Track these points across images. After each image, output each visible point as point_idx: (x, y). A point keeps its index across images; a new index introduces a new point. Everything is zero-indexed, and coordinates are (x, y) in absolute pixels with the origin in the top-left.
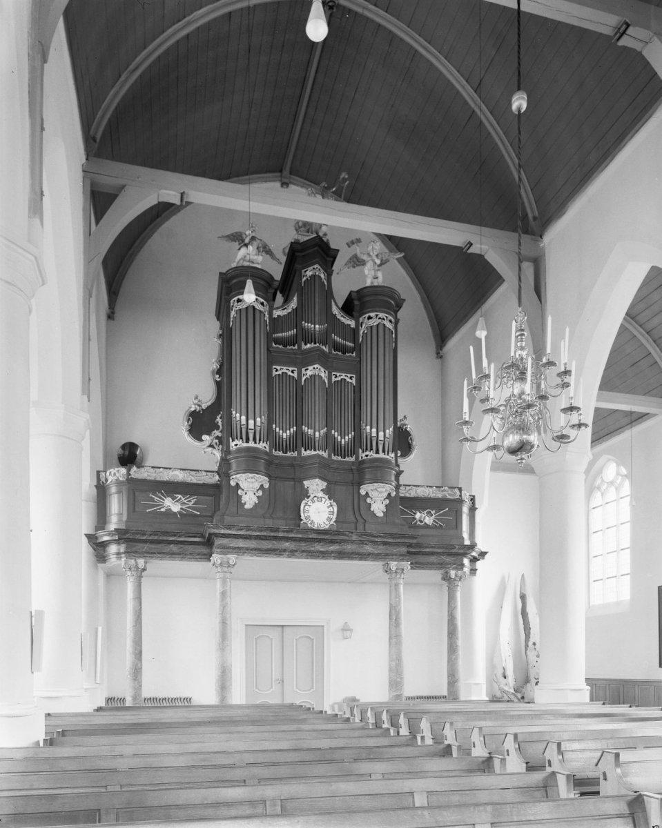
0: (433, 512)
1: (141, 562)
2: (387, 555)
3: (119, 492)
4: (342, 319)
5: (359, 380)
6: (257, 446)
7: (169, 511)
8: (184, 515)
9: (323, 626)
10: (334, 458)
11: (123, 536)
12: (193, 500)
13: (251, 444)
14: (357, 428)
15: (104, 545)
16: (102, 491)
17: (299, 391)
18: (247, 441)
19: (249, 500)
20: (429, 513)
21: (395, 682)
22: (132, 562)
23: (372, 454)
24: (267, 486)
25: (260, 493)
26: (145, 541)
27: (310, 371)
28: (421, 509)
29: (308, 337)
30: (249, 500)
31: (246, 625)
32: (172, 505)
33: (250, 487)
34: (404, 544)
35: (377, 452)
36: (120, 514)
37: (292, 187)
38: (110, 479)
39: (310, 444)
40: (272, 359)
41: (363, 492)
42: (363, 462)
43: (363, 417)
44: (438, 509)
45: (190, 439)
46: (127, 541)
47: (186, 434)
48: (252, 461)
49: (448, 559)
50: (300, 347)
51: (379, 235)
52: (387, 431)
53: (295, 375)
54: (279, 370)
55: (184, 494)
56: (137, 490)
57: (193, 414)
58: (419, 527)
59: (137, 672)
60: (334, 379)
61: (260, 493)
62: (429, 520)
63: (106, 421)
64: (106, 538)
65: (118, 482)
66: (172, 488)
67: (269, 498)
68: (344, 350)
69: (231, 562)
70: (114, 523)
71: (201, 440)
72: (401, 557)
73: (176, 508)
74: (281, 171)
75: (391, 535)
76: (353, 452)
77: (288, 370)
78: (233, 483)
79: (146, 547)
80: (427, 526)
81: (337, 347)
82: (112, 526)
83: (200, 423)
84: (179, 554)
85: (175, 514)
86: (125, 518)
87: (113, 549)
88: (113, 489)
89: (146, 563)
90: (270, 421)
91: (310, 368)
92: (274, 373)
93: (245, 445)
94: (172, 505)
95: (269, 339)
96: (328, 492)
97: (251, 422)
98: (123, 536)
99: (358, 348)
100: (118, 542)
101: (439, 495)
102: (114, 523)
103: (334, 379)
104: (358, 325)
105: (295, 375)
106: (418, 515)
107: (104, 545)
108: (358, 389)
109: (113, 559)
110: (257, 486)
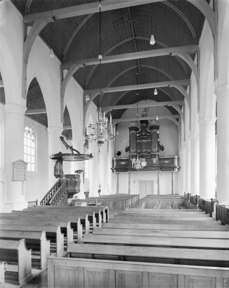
1: (118, 172)
5: (151, 141)
7: (122, 164)
8: (125, 164)
10: (147, 154)
11: (115, 168)
12: (126, 162)
13: (133, 154)
16: (113, 161)
17: (141, 144)
20: (168, 161)
21: (129, 191)
22: (117, 172)
23: (153, 153)
26: (119, 169)
27: (142, 141)
28: (165, 160)
29: (142, 135)
31: (139, 181)
37: (147, 100)
38: (114, 159)
39: (143, 153)
40: (137, 139)
41: (152, 160)
42: (152, 155)
43: (152, 147)
47: (125, 151)
49: (171, 169)
51: (164, 106)
53: (141, 141)
55: (125, 161)
56: (118, 161)
59: (118, 190)
60: (147, 141)
62: (167, 162)
64: (114, 169)
65: (115, 160)
68: (149, 136)
69: (130, 172)
70: (115, 167)
72: (159, 170)
73: (123, 164)
74: (144, 98)
77: (140, 141)
78: (131, 160)
79: (119, 170)
80: (167, 163)
81: (147, 136)
82: (115, 167)
85: (123, 165)
87: (115, 170)
88: (115, 161)
90: (137, 149)
92: (137, 142)
93: (132, 154)
96: (146, 161)
97: (133, 151)
98: (115, 168)
99: (151, 135)
100: (115, 169)
101: (170, 157)
103: (147, 141)
104: (151, 131)
105: (141, 141)
106: (165, 161)
108: (151, 142)
109: (115, 172)
110: (156, 160)
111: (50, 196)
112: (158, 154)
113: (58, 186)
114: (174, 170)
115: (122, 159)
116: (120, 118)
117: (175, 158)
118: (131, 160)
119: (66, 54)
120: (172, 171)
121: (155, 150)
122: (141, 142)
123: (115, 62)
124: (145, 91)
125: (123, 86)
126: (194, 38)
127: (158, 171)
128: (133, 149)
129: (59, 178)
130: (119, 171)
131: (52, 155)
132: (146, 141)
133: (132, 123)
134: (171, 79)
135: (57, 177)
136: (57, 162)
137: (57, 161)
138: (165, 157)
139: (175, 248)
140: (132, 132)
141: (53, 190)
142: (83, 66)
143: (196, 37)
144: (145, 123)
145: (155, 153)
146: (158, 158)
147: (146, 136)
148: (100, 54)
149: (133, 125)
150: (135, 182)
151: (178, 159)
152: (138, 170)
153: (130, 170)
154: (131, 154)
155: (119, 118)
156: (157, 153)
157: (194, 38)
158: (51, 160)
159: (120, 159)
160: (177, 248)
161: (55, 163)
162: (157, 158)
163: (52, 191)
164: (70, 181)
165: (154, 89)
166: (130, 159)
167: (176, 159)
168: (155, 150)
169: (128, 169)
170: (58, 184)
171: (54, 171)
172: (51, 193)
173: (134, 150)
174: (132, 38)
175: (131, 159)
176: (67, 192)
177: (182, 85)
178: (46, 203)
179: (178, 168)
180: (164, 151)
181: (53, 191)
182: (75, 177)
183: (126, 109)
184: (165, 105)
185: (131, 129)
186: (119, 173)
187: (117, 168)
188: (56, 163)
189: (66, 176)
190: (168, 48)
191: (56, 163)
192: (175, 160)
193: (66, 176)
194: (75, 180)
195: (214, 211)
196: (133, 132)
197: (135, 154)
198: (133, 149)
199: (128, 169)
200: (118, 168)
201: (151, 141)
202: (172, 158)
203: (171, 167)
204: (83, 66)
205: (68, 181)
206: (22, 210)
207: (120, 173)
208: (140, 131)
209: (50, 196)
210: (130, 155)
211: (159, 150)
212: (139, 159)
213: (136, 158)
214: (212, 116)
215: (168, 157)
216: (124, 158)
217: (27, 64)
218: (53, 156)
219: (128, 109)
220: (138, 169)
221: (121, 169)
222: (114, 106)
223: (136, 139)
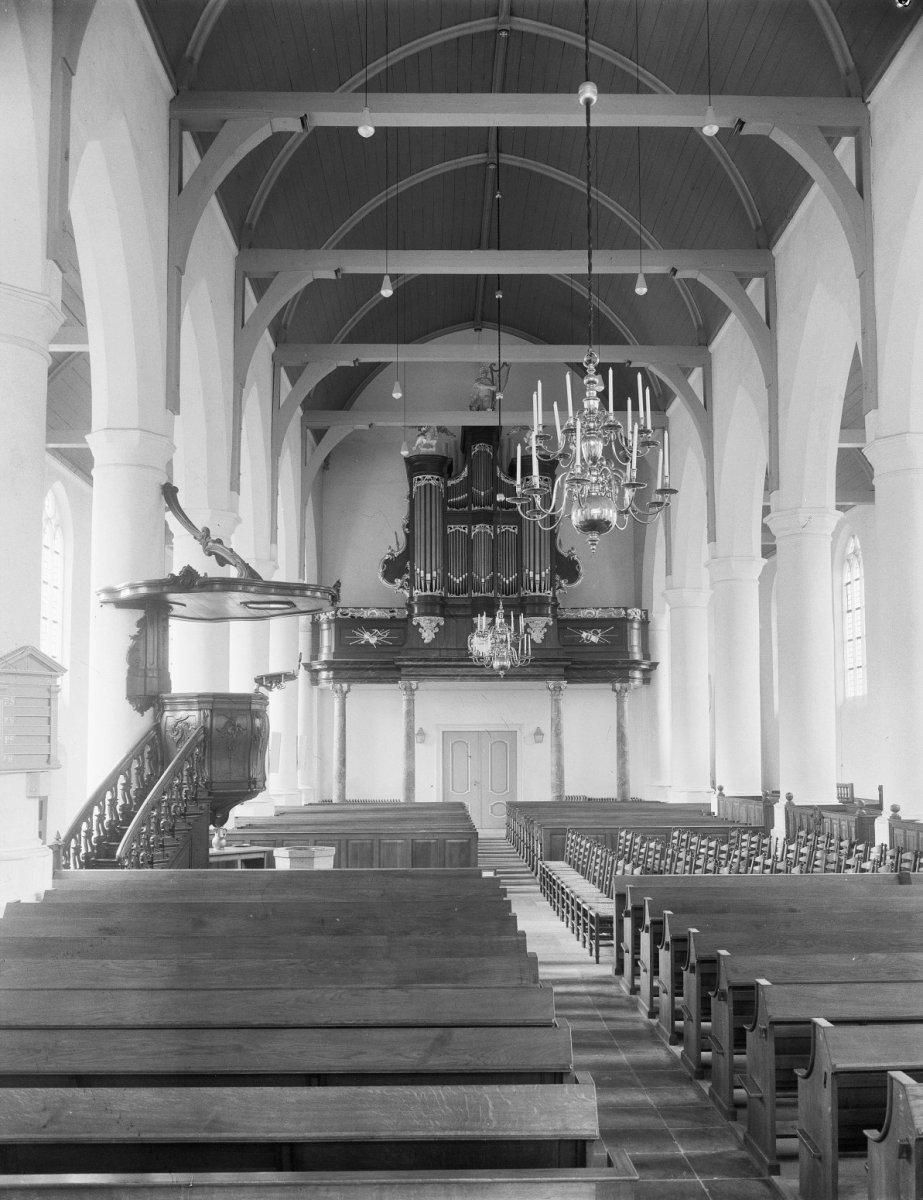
0: (599, 631)
1: (345, 686)
2: (545, 675)
3: (329, 629)
4: (506, 481)
6: (434, 593)
7: (367, 643)
9: (443, 732)
11: (329, 666)
12: (387, 632)
13: (428, 593)
14: (520, 569)
15: (317, 671)
18: (425, 590)
19: (428, 636)
20: (596, 633)
24: (442, 623)
25: (437, 630)
28: (587, 629)
30: (428, 636)
31: (443, 732)
32: (370, 638)
33: (428, 628)
34: (561, 666)
35: (535, 591)
36: (329, 647)
40: (447, 519)
42: (523, 599)
44: (603, 629)
45: (384, 582)
46: (334, 669)
48: (431, 606)
50: (470, 509)
51: (567, 364)
52: (543, 573)
54: (452, 529)
57: (387, 562)
58: (585, 645)
61: (437, 630)
62: (594, 639)
63: (433, 1074)
64: (318, 667)
65: (329, 622)
66: (371, 624)
67: (442, 633)
69: (414, 687)
70: (324, 656)
71: (393, 582)
73: (373, 640)
75: (547, 660)
76: (517, 590)
79: (350, 673)
83: (394, 568)
84: (376, 678)
86: (333, 651)
87: (324, 674)
88: (325, 626)
89: (349, 686)
90: (446, 570)
91: (478, 526)
92: (449, 531)
93: (423, 594)
94: (370, 638)
95: (445, 503)
98: (329, 666)
100: (328, 670)
102: (324, 656)
106: (584, 635)
107: (317, 671)
108: (519, 537)
109: (324, 684)
110: (434, 624)
111: (107, 812)
112: (554, 598)
113: (146, 755)
114: (627, 679)
115: (366, 614)
116: (348, 409)
117: (632, 621)
118: (415, 623)
119: (200, 49)
120: (618, 686)
121: (537, 577)
122: (470, 532)
123: (630, 128)
124: (485, 282)
125: (357, 248)
126: (843, 70)
127: (551, 684)
128: (428, 570)
129: (149, 713)
130: (351, 680)
131: (133, 587)
132: (495, 531)
133: (423, 434)
134: (648, 242)
135: (141, 710)
136: (141, 623)
137: (145, 617)
138: (583, 614)
139: (309, 1084)
140: (423, 483)
141: (122, 780)
142: (294, 125)
143: (851, 64)
144: (489, 441)
145: (538, 593)
146: (554, 617)
147: (495, 508)
148: (587, 80)
149: (426, 445)
150: (424, 734)
151: (645, 623)
152: (502, 673)
153: (409, 676)
154: (417, 592)
155: (341, 409)
156: (549, 593)
157: (843, 70)
158: (110, 609)
159: (357, 615)
160: (326, 1084)
161: (135, 630)
162: (547, 615)
163: (115, 785)
164: (225, 727)
165: (634, 277)
166: (410, 616)
167: (636, 625)
168: (537, 577)
169: (398, 668)
170: (148, 749)
171: (129, 672)
172: (109, 796)
173: (434, 573)
174: (497, 22)
175: (418, 615)
176: (210, 794)
177: (737, 274)
178: (87, 856)
179: (644, 667)
180: (579, 582)
181: (120, 787)
182: (253, 707)
183: (379, 363)
184: (568, 361)
185: (416, 465)
186: (349, 690)
187: (342, 662)
188: (138, 629)
189: (199, 702)
190: (666, 92)
191: (138, 629)
192: (632, 628)
193: (199, 702)
194: (253, 724)
195: (9, 906)
196: (433, 482)
197: (437, 593)
198: (428, 570)
199: (398, 668)
200: (347, 663)
201: (520, 531)
202: (619, 619)
203: (612, 665)
204: (294, 125)
205: (214, 731)
206: (33, 900)
207: (354, 687)
208: (465, 478)
209: (107, 812)
210: (411, 598)
211: (557, 577)
212: (507, 617)
213: (492, 615)
214: (911, 430)
215: (597, 614)
216: (377, 614)
217: (73, 74)
218: (143, 591)
219: (386, 364)
220: (502, 668)
221: (358, 669)
222: (338, 345)
223: (445, 515)
